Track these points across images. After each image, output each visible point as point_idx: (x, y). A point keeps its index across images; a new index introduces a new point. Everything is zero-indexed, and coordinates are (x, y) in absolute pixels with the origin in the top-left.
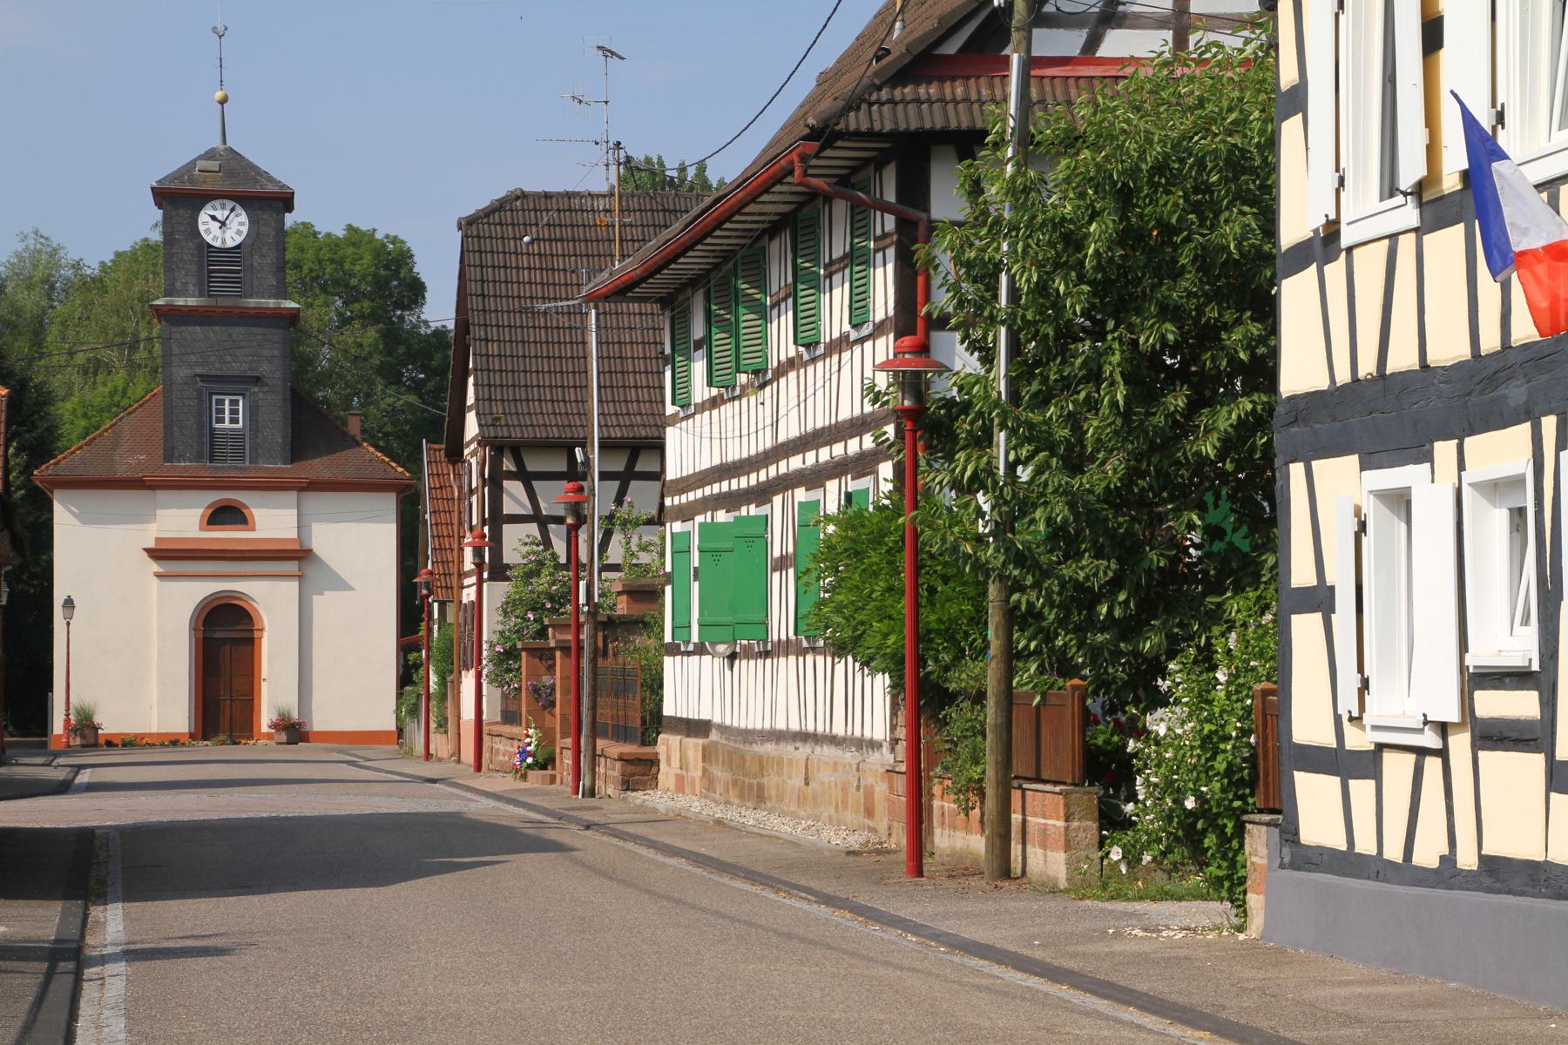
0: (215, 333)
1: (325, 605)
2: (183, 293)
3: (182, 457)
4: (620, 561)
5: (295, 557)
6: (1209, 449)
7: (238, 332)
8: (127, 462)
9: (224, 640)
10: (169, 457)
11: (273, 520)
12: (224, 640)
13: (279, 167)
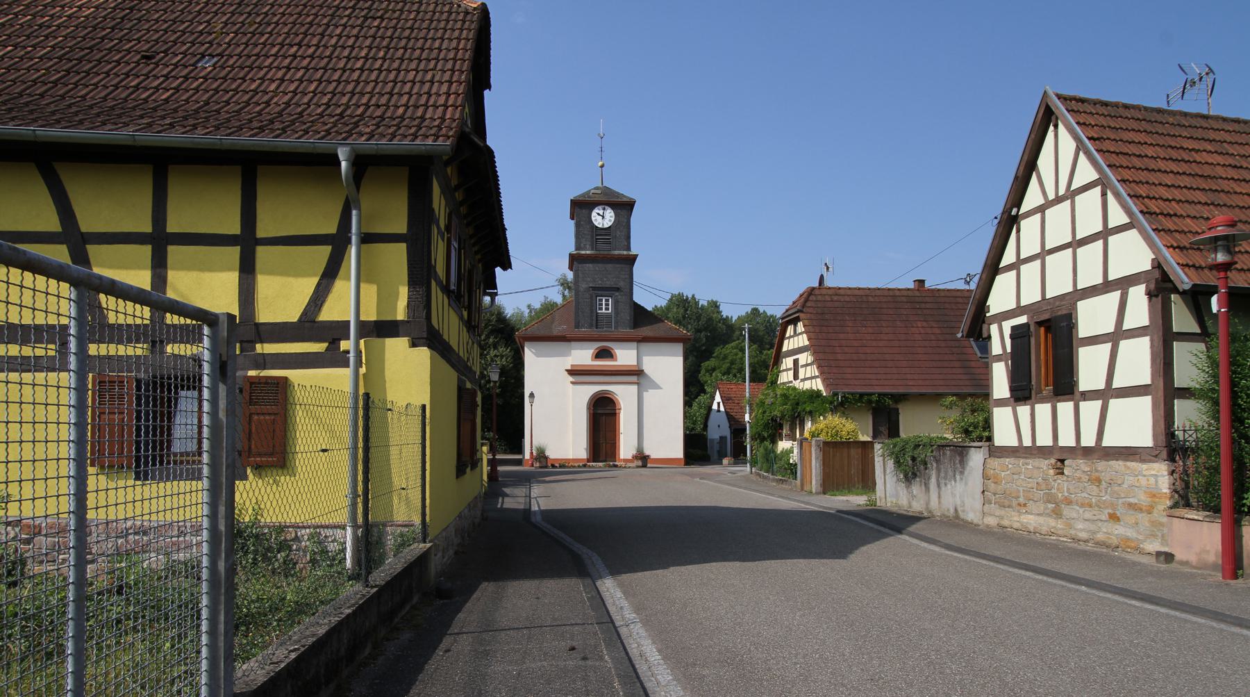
0: (599, 267)
1: (649, 396)
2: (585, 249)
3: (583, 326)
4: (903, 435)
5: (636, 374)
6: (168, 321)
7: (609, 266)
8: (557, 329)
9: (602, 414)
10: (577, 326)
11: (625, 356)
12: (602, 414)
13: (625, 189)
